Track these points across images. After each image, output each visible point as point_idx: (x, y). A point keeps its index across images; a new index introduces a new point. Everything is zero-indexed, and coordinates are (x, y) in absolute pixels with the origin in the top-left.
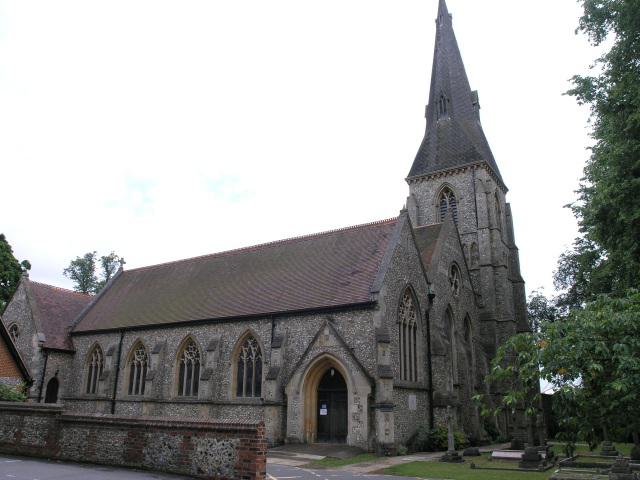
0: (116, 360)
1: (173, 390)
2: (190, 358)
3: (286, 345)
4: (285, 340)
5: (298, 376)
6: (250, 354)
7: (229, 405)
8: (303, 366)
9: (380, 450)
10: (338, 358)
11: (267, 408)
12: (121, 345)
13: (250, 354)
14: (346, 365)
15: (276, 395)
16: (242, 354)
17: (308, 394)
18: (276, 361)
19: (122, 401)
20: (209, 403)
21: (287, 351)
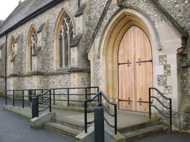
0: (4, 52)
1: (27, 67)
2: (34, 42)
3: (89, 12)
4: (88, 7)
5: (97, 40)
6: (66, 30)
7: (53, 74)
8: (102, 29)
9: (53, 121)
10: (137, 10)
11: (72, 75)
12: (6, 42)
13: (66, 30)
14: (147, 17)
15: (79, 62)
16: (61, 32)
17: (110, 59)
18: (79, 29)
19: (146, 102)
20: (38, 74)
21: (90, 18)
